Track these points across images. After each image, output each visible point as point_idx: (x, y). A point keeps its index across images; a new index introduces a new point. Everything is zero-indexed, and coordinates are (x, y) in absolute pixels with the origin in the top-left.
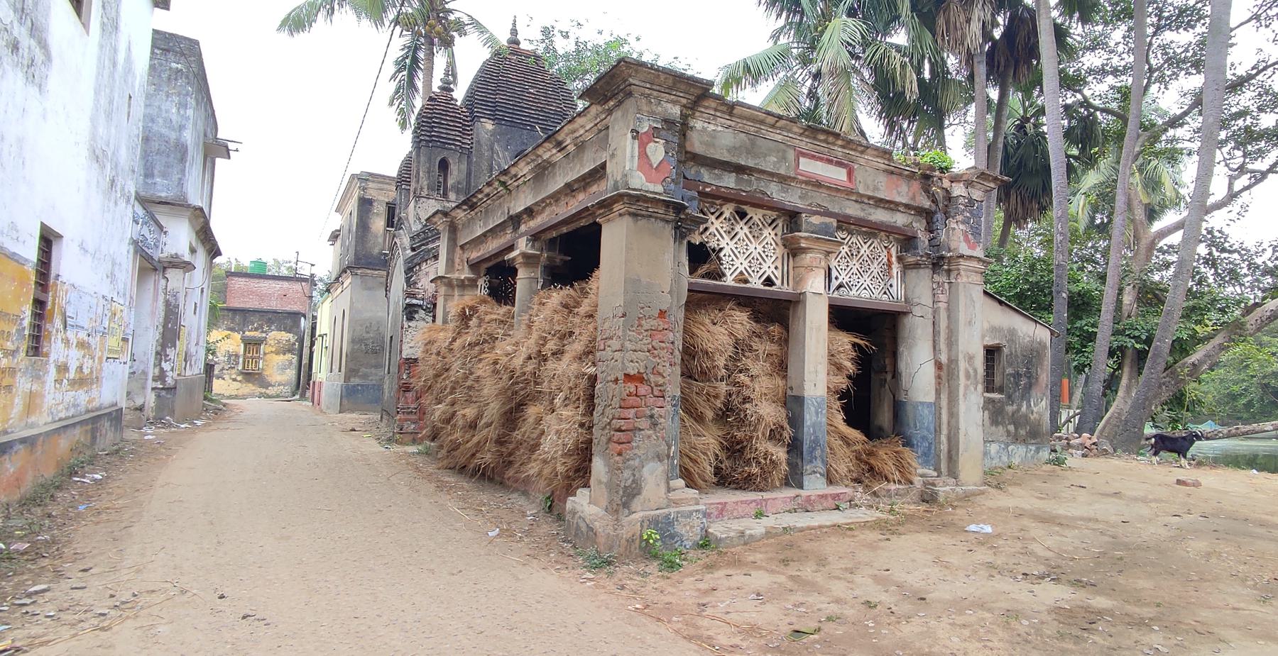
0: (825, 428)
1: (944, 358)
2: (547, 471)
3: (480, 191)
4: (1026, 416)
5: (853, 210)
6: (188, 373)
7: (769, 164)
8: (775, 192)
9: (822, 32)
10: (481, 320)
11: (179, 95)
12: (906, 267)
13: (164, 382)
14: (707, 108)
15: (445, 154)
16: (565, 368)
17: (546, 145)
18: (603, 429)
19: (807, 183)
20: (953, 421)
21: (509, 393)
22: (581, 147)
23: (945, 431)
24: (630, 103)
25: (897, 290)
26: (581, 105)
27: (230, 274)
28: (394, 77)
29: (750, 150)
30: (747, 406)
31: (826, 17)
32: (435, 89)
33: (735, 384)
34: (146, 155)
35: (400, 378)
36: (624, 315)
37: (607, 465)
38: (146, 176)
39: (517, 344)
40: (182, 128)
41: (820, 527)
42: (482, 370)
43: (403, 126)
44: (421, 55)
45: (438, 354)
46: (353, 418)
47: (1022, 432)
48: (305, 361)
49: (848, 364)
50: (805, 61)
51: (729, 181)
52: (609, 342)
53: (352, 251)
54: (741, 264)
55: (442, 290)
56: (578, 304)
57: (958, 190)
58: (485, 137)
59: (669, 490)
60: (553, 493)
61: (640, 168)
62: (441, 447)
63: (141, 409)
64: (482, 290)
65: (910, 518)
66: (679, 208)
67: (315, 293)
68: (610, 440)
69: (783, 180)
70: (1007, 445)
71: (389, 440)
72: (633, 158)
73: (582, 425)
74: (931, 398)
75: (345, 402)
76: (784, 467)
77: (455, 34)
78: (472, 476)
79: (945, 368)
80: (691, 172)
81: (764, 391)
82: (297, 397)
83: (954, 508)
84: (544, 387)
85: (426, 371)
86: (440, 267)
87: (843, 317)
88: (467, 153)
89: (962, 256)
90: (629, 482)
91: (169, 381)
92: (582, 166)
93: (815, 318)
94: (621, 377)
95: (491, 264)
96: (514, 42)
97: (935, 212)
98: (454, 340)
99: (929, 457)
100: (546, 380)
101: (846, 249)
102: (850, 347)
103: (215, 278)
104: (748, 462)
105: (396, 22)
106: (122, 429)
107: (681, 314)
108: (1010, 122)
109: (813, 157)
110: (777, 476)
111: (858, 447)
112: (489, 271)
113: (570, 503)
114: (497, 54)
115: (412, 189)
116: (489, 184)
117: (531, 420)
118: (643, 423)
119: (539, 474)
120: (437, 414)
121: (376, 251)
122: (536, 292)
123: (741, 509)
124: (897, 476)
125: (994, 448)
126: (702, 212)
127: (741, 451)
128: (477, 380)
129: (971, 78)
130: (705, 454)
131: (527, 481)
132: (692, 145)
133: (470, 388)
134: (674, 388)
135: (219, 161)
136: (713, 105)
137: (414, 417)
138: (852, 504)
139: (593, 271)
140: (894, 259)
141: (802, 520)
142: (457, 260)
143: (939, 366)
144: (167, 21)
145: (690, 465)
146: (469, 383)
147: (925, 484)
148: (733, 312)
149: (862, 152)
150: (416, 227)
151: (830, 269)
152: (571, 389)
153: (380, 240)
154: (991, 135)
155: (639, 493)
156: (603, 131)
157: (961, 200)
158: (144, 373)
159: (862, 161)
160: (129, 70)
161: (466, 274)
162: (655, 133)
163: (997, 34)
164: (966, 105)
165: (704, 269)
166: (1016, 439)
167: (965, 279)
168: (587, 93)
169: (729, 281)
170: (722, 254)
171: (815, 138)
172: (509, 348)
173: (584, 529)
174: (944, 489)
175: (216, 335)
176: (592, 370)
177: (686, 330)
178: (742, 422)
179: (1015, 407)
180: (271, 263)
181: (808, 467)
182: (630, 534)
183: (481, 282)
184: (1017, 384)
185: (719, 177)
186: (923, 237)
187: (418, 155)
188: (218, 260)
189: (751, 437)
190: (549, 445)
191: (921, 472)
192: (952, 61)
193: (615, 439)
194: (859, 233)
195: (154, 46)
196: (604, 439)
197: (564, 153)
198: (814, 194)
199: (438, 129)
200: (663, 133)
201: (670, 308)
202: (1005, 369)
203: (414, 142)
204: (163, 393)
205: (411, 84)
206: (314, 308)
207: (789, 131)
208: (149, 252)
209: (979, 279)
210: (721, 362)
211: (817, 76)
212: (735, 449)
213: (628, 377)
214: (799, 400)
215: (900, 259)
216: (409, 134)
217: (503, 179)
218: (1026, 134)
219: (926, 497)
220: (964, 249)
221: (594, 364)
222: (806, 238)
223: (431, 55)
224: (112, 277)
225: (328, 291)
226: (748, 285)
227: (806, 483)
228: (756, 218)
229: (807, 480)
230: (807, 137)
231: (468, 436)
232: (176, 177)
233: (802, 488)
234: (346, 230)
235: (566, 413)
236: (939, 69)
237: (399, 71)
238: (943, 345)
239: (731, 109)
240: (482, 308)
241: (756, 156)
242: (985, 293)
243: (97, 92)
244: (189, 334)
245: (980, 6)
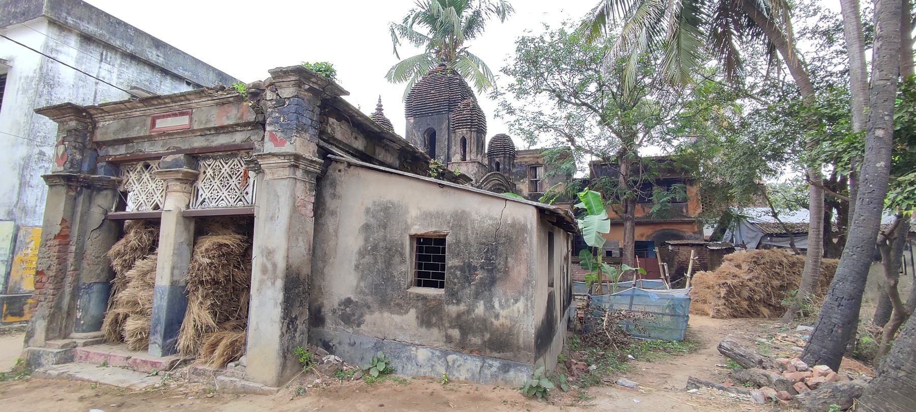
5: (198, 143)
29: (126, 128)
41: (88, 381)
51: (122, 150)
69: (150, 138)
70: (446, 354)
109: (164, 117)
123: (96, 358)
166: (462, 347)
185: (117, 150)
194: (221, 157)
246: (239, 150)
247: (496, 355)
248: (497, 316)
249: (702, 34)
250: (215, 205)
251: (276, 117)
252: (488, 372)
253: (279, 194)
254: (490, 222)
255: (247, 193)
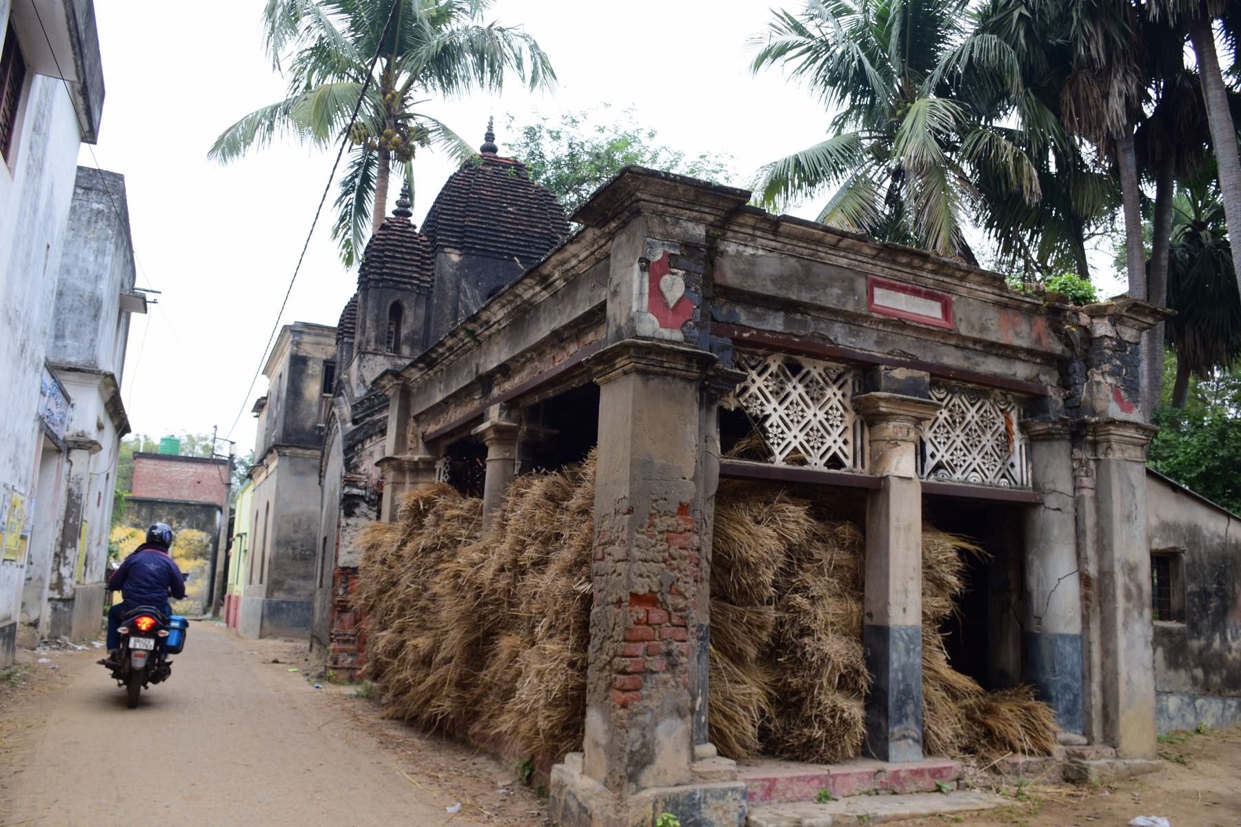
0: (920, 672)
1: (1092, 570)
2: (524, 727)
3: (441, 344)
4: (1220, 656)
5: (952, 358)
6: (88, 581)
7: (831, 297)
8: (840, 335)
9: (903, 117)
10: (439, 517)
11: (98, 239)
12: (1033, 440)
13: (61, 591)
14: (742, 225)
15: (399, 296)
16: (549, 583)
17: (528, 281)
18: (601, 670)
19: (886, 322)
20: (1109, 662)
21: (475, 617)
22: (573, 282)
23: (1097, 677)
24: (637, 225)
25: (1021, 470)
26: (574, 226)
27: (138, 456)
28: (340, 200)
29: (805, 279)
30: (806, 640)
31: (907, 97)
32: (389, 214)
33: (788, 608)
34: (58, 312)
35: (335, 594)
36: (630, 511)
37: (607, 720)
38: (57, 337)
39: (485, 550)
40: (98, 278)
42: (440, 585)
43: (349, 261)
44: (374, 171)
45: (383, 562)
46: (276, 646)
47: (1216, 679)
48: (220, 568)
49: (953, 580)
50: (880, 155)
51: (776, 323)
52: (610, 549)
53: (280, 425)
54: (795, 437)
55: (390, 476)
56: (568, 496)
57: (1102, 328)
58: (449, 271)
59: (694, 758)
60: (532, 758)
61: (652, 309)
62: (385, 689)
63: (35, 624)
64: (440, 477)
65: (1046, 805)
66: (706, 362)
67: (234, 480)
68: (610, 686)
69: (853, 320)
70: (1193, 698)
71: (321, 677)
72: (642, 298)
73: (572, 664)
74: (1075, 628)
75: (267, 624)
76: (861, 728)
77: (415, 143)
78: (425, 730)
79: (1095, 584)
80: (722, 312)
81: (830, 618)
82: (209, 615)
83: (1113, 790)
84: (522, 610)
85: (367, 586)
86: (388, 445)
87: (942, 510)
88: (425, 294)
89: (1112, 422)
90: (637, 746)
91: (68, 591)
92: (574, 307)
93: (904, 511)
94: (625, 595)
95: (453, 440)
96: (489, 148)
97: (1070, 361)
98: (404, 543)
99: (1074, 715)
100: (525, 600)
101: (946, 413)
102: (954, 554)
103: (122, 460)
104: (808, 723)
105: (348, 131)
106: (14, 649)
107: (710, 510)
108: (1177, 229)
109: (892, 287)
110: (850, 743)
111: (971, 701)
112: (450, 451)
113: (557, 772)
114: (467, 165)
115: (356, 342)
116: (453, 334)
117: (504, 656)
118: (657, 663)
119: (515, 730)
120: (381, 643)
121: (309, 424)
122: (512, 479)
124: (1028, 743)
125: (1173, 703)
126: (738, 365)
127: (799, 705)
128: (434, 598)
129: (1115, 171)
130: (745, 708)
131: (498, 740)
132: (723, 276)
133: (424, 609)
134: (700, 616)
135: (135, 316)
136: (751, 221)
137: (351, 647)
138: (961, 783)
139: (588, 450)
140: (1015, 427)
141: (885, 807)
142: (410, 436)
143: (1085, 580)
144: (89, 156)
145: (724, 724)
146: (422, 603)
147: (1069, 755)
148: (784, 506)
149: (962, 279)
150: (359, 393)
151: (923, 444)
152: (557, 613)
153: (315, 409)
154: (1149, 246)
155: (651, 761)
156: (601, 266)
157: (1107, 343)
158: (41, 579)
159: (962, 291)
160: (49, 216)
161: (420, 455)
162: (671, 262)
163: (1148, 110)
164: (1111, 208)
165: (744, 444)
166: (1207, 689)
167: (1118, 455)
168: (585, 212)
169: (779, 461)
170: (767, 424)
171: (894, 262)
172: (476, 556)
173: (575, 809)
174: (1098, 762)
175: (120, 532)
176: (586, 587)
177: (718, 532)
178: (799, 662)
179: (1202, 642)
180: (184, 440)
181: (896, 730)
182: (638, 819)
183: (439, 465)
184: (1205, 608)
185: (761, 318)
186: (1055, 396)
187: (365, 299)
188: (127, 438)
189: (812, 686)
190: (528, 691)
191: (1063, 738)
192: (1087, 151)
193: (618, 684)
195: (77, 185)
196: (602, 684)
197: (551, 291)
198: (896, 337)
199: (391, 265)
200: (683, 261)
201: (694, 501)
202: (1186, 587)
203: (360, 283)
204: (60, 605)
205: (360, 209)
206: (232, 498)
207: (857, 253)
208: (54, 429)
209: (1137, 453)
210: (768, 576)
211: (898, 174)
212: (789, 703)
213: (636, 598)
214: (882, 633)
215: (1023, 427)
216: (354, 273)
217: (470, 326)
218: (1201, 245)
219: (1070, 774)
220: (1115, 411)
221: (589, 579)
222: (887, 400)
223: (385, 172)
224: (14, 460)
225: (250, 476)
226: (806, 467)
227: (892, 752)
228: (814, 373)
229: (894, 749)
230: (883, 260)
231: (420, 675)
232: (87, 338)
233: (885, 757)
234: (275, 394)
235: (551, 647)
236: (1069, 158)
237: (346, 193)
238: (1090, 551)
239: (776, 225)
240: (441, 501)
241: (811, 287)
242: (1149, 473)
243: (15, 244)
244: (91, 532)
245: (1119, 77)
246: (994, 387)
247: (1233, 693)
248: (1230, 649)
249: (357, 109)
250: (962, 478)
251: (1117, 366)
252: (1228, 714)
253: (1134, 483)
254: (1217, 540)
255: (1012, 465)
